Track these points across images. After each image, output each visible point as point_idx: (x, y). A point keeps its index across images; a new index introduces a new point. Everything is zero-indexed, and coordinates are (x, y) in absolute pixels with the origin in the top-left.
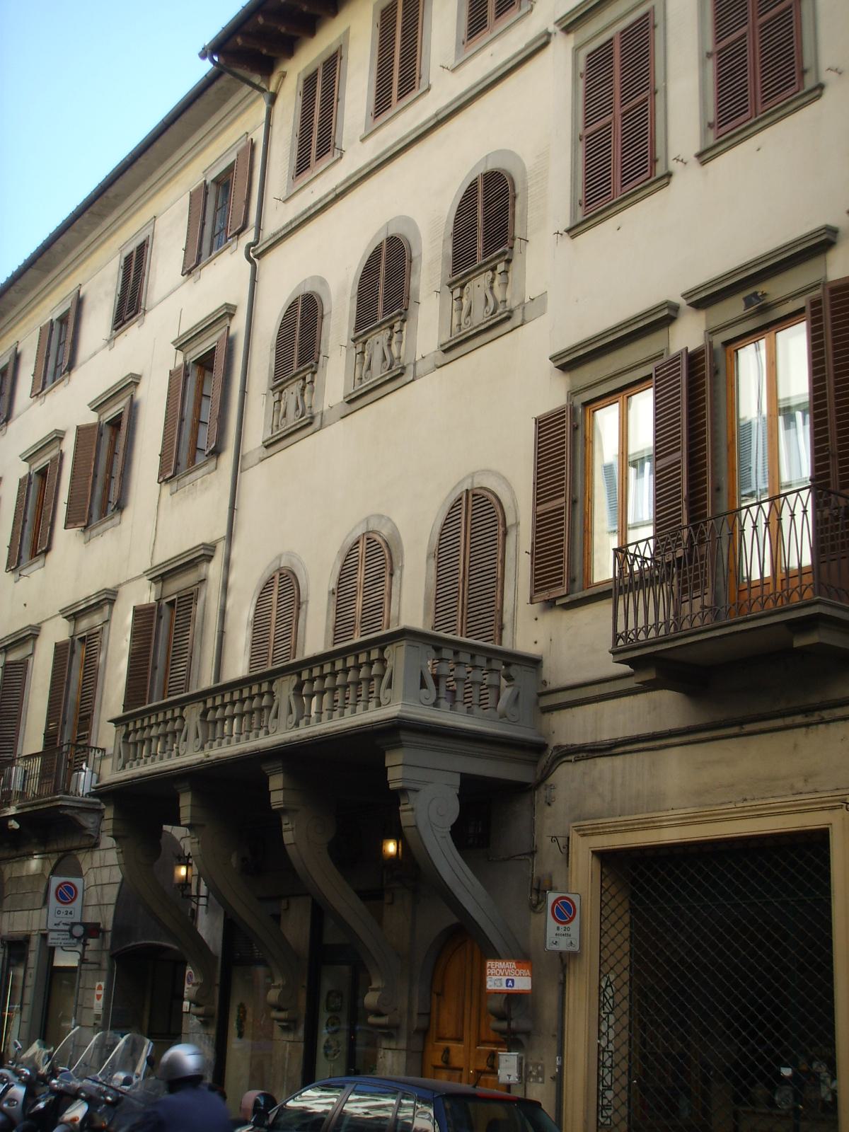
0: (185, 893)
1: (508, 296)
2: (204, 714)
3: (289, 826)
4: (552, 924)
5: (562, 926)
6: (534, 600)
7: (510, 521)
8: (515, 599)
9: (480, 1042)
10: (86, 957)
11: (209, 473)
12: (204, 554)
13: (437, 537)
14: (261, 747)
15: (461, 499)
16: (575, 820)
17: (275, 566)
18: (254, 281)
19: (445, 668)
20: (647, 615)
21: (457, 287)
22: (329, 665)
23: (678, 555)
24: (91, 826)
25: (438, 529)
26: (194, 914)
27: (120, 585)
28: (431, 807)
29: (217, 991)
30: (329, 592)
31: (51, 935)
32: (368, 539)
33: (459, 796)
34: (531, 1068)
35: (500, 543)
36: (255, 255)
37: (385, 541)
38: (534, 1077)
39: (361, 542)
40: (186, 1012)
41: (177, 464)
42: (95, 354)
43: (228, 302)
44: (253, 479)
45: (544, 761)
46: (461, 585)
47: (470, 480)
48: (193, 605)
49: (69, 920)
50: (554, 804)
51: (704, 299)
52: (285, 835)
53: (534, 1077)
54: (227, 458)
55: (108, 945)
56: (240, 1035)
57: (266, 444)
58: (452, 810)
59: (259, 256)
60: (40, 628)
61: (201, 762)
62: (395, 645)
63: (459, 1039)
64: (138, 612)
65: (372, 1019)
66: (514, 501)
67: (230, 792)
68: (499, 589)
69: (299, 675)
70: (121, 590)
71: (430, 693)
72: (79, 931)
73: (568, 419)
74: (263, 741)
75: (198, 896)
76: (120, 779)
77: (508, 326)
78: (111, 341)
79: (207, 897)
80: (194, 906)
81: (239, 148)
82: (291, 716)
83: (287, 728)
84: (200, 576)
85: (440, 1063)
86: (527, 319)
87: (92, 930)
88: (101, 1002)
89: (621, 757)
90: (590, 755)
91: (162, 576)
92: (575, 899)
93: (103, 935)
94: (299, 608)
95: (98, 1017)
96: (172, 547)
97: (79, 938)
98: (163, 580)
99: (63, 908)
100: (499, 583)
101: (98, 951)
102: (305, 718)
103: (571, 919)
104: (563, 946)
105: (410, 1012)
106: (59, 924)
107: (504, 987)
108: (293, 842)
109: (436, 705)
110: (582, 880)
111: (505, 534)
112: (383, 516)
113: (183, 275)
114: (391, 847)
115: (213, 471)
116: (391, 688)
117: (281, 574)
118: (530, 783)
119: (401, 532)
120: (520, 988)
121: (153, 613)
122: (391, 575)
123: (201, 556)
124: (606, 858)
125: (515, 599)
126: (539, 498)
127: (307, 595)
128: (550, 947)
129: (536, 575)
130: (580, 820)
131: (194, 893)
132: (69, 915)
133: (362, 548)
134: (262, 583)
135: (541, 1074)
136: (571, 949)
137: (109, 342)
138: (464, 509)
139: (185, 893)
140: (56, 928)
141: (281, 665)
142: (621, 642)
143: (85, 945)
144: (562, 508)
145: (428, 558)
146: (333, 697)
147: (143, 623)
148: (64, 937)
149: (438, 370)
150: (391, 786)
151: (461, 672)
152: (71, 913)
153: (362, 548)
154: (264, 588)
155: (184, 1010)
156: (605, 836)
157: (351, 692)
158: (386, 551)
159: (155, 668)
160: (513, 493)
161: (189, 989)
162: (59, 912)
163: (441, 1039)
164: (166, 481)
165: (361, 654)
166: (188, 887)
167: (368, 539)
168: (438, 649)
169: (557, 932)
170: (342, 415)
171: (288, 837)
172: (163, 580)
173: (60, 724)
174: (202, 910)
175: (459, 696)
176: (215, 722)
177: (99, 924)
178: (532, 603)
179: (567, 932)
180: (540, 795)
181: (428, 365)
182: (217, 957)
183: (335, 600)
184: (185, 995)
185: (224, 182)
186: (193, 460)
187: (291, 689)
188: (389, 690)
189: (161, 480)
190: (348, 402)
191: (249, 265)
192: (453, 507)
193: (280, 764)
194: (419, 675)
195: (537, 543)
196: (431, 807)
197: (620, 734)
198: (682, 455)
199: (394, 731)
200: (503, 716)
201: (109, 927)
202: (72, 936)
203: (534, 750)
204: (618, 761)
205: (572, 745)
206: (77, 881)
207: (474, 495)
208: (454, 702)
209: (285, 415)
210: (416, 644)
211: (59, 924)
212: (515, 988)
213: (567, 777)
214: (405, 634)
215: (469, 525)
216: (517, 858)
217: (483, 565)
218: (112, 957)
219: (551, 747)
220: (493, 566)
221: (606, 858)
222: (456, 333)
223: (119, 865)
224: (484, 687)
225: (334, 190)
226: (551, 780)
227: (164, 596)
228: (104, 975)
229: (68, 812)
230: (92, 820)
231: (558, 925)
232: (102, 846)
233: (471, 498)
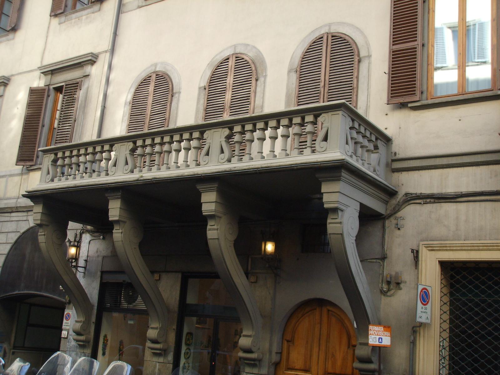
5: (424, 307)
7: (363, 53)
11: (93, 13)
12: (92, 60)
14: (200, 172)
22: (76, 151)
27: (13, 75)
30: (200, 88)
32: (236, 57)
39: (231, 59)
41: (66, 6)
45: (394, 202)
46: (322, 90)
48: (78, 90)
50: (402, 230)
52: (39, 237)
56: (104, 354)
60: (98, 56)
61: (137, 180)
62: (213, 131)
64: (33, 92)
65: (241, 354)
68: (355, 94)
69: (56, 154)
70: (13, 78)
76: (54, 187)
82: (49, 175)
83: (218, 162)
84: (85, 73)
89: (465, 204)
90: (436, 201)
91: (52, 71)
96: (59, 54)
98: (52, 74)
100: (355, 90)
102: (58, 177)
105: (270, 352)
107: (377, 343)
108: (217, 238)
110: (431, 276)
111: (359, 61)
112: (248, 45)
115: (96, 12)
116: (49, 174)
120: (385, 344)
121: (44, 92)
127: (180, 89)
130: (427, 241)
146: (150, 159)
147: (36, 98)
154: (142, 83)
155: (63, 336)
156: (447, 252)
157: (148, 159)
159: (43, 126)
160: (365, 37)
164: (56, 16)
167: (236, 57)
172: (52, 74)
179: (425, 311)
180: (390, 224)
182: (93, 306)
183: (207, 93)
186: (74, 6)
187: (50, 161)
192: (314, 42)
193: (217, 185)
197: (464, 189)
199: (335, 170)
204: (462, 207)
205: (421, 194)
207: (332, 36)
212: (383, 344)
213: (412, 214)
216: (369, 260)
226: (400, 214)
227: (52, 83)
233: (330, 38)
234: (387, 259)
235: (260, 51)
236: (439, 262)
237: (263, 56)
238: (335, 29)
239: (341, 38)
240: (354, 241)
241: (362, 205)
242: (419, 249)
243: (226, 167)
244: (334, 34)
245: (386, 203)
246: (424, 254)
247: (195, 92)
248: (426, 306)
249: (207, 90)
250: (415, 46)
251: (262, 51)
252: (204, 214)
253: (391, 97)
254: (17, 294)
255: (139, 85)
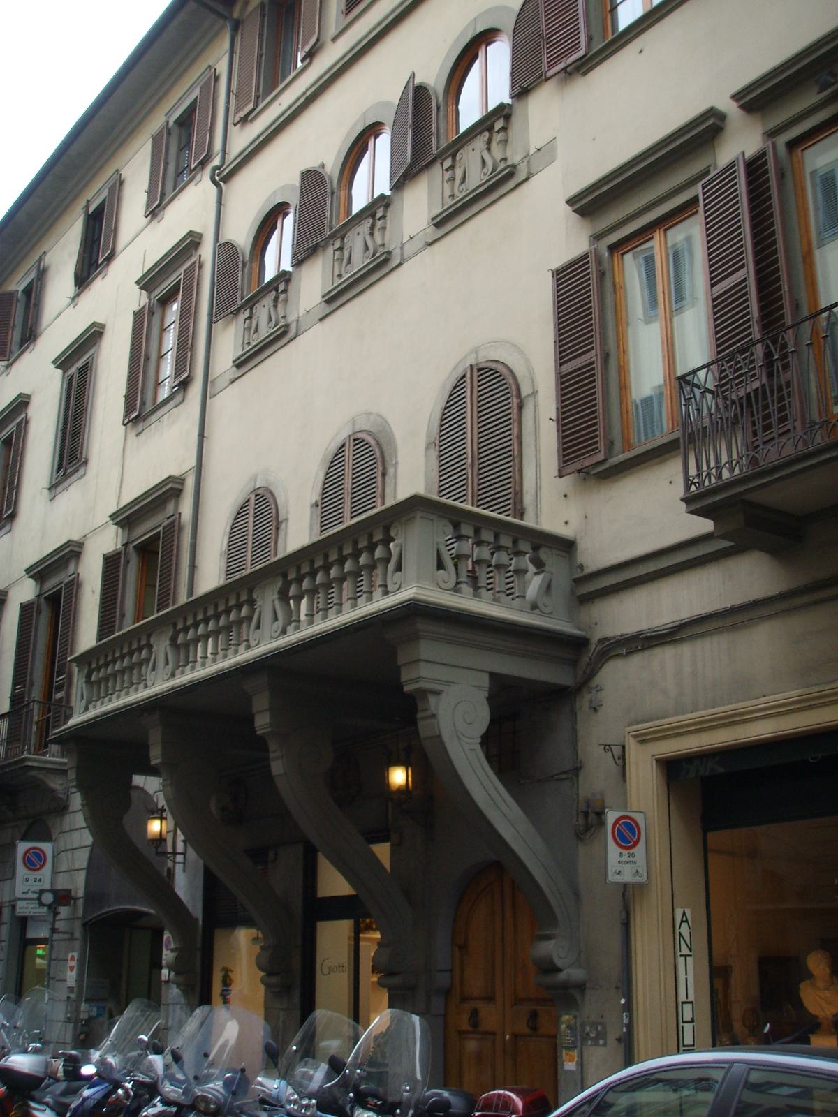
0: (160, 850)
1: (509, 154)
2: (173, 640)
3: (278, 754)
4: (613, 850)
5: (625, 852)
6: (564, 473)
7: (525, 391)
8: (538, 477)
9: (517, 1001)
10: (56, 927)
11: (176, 406)
13: (437, 423)
15: (464, 376)
16: (630, 724)
17: (250, 488)
18: (220, 204)
19: (466, 546)
20: (725, 460)
21: (448, 156)
23: (748, 391)
24: (58, 787)
25: (438, 415)
26: (171, 874)
28: (458, 713)
29: (199, 954)
31: (20, 904)
33: (488, 699)
34: (588, 1029)
35: (515, 417)
36: (223, 178)
37: (378, 444)
38: (592, 1039)
40: (165, 981)
42: (60, 314)
43: (193, 229)
44: (226, 404)
46: (470, 471)
47: (474, 356)
49: (37, 887)
51: (757, 99)
53: (592, 1039)
54: (195, 390)
55: (80, 912)
57: (237, 362)
58: (481, 717)
59: (227, 179)
63: (490, 999)
66: (531, 372)
67: (205, 728)
71: (449, 576)
72: (48, 898)
73: (593, 265)
74: (244, 656)
75: (175, 853)
77: (511, 184)
78: (75, 299)
79: (184, 854)
80: (170, 864)
81: (202, 83)
85: (466, 1026)
86: (533, 171)
87: (63, 897)
88: (74, 973)
92: (639, 818)
93: (75, 902)
94: (278, 529)
95: (71, 990)
97: (49, 906)
99: (32, 875)
101: (71, 919)
103: (636, 843)
104: (628, 876)
106: (27, 892)
109: (456, 589)
110: (644, 792)
111: (521, 407)
112: (370, 413)
113: (146, 217)
114: (398, 776)
115: (180, 403)
117: (256, 496)
118: (568, 687)
119: (392, 426)
122: (384, 475)
123: (169, 491)
124: (672, 768)
125: (538, 477)
126: (563, 356)
127: (287, 513)
128: (612, 877)
129: (564, 444)
131: (170, 849)
132: (38, 883)
133: (348, 453)
134: (237, 507)
135: (602, 1035)
136: (638, 879)
137: (73, 299)
138: (469, 386)
139: (160, 850)
140: (24, 896)
141: (261, 566)
142: (693, 488)
143: (56, 914)
144: (593, 363)
145: (427, 448)
148: (32, 906)
149: (429, 248)
150: (406, 689)
151: (484, 552)
152: (40, 880)
153: (348, 453)
155: (163, 978)
158: (377, 450)
161: (167, 955)
162: (27, 880)
163: (465, 999)
165: (360, 536)
166: (163, 843)
167: (355, 440)
168: (456, 526)
169: (620, 859)
170: (321, 316)
171: (277, 768)
173: (27, 686)
174: (179, 869)
175: (483, 581)
176: (186, 645)
177: (69, 891)
178: (561, 476)
179: (631, 859)
180: (584, 701)
181: (418, 244)
182: (197, 920)
183: (319, 512)
184: (164, 962)
185: (186, 121)
188: (398, 573)
189: (126, 421)
190: (326, 302)
191: (214, 189)
194: (435, 558)
195: (563, 407)
196: (458, 713)
197: (685, 614)
198: (748, 273)
200: (534, 607)
201: (81, 893)
202: (41, 904)
203: (571, 648)
204: (686, 650)
206: (47, 847)
207: (479, 370)
208: (476, 588)
209: (256, 331)
210: (431, 516)
211: (27, 892)
214: (415, 504)
215: (475, 408)
216: (556, 777)
217: (494, 444)
218: (85, 925)
219: (594, 640)
220: (509, 443)
221: (672, 768)
222: (449, 202)
223: (87, 827)
224: (510, 574)
225: (304, 93)
226: (597, 680)
228: (77, 944)
229: (34, 773)
230: (61, 782)
231: (620, 850)
232: (71, 809)
234: (583, 770)
235: (386, 421)
236: (657, 760)
237: (390, 428)
238: (484, 356)
239: (491, 370)
240: (479, 746)
241: (492, 675)
242: (624, 742)
243: (282, 642)
244: (481, 366)
245: (574, 663)
246: (633, 748)
247: (307, 512)
248: (631, 851)
249: (320, 507)
250: (592, 360)
251: (390, 421)
252: (258, 733)
253: (565, 462)
254: (106, 913)
255: (235, 519)
